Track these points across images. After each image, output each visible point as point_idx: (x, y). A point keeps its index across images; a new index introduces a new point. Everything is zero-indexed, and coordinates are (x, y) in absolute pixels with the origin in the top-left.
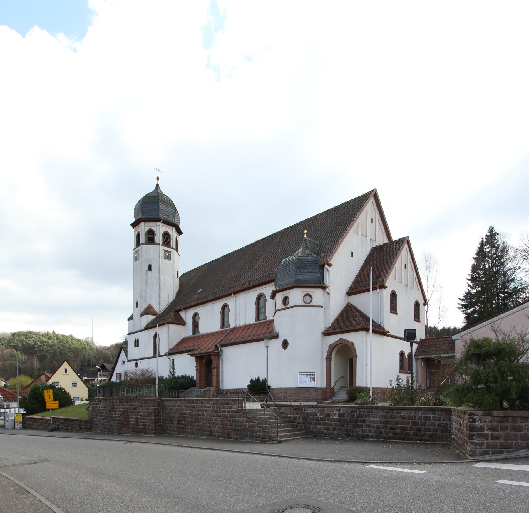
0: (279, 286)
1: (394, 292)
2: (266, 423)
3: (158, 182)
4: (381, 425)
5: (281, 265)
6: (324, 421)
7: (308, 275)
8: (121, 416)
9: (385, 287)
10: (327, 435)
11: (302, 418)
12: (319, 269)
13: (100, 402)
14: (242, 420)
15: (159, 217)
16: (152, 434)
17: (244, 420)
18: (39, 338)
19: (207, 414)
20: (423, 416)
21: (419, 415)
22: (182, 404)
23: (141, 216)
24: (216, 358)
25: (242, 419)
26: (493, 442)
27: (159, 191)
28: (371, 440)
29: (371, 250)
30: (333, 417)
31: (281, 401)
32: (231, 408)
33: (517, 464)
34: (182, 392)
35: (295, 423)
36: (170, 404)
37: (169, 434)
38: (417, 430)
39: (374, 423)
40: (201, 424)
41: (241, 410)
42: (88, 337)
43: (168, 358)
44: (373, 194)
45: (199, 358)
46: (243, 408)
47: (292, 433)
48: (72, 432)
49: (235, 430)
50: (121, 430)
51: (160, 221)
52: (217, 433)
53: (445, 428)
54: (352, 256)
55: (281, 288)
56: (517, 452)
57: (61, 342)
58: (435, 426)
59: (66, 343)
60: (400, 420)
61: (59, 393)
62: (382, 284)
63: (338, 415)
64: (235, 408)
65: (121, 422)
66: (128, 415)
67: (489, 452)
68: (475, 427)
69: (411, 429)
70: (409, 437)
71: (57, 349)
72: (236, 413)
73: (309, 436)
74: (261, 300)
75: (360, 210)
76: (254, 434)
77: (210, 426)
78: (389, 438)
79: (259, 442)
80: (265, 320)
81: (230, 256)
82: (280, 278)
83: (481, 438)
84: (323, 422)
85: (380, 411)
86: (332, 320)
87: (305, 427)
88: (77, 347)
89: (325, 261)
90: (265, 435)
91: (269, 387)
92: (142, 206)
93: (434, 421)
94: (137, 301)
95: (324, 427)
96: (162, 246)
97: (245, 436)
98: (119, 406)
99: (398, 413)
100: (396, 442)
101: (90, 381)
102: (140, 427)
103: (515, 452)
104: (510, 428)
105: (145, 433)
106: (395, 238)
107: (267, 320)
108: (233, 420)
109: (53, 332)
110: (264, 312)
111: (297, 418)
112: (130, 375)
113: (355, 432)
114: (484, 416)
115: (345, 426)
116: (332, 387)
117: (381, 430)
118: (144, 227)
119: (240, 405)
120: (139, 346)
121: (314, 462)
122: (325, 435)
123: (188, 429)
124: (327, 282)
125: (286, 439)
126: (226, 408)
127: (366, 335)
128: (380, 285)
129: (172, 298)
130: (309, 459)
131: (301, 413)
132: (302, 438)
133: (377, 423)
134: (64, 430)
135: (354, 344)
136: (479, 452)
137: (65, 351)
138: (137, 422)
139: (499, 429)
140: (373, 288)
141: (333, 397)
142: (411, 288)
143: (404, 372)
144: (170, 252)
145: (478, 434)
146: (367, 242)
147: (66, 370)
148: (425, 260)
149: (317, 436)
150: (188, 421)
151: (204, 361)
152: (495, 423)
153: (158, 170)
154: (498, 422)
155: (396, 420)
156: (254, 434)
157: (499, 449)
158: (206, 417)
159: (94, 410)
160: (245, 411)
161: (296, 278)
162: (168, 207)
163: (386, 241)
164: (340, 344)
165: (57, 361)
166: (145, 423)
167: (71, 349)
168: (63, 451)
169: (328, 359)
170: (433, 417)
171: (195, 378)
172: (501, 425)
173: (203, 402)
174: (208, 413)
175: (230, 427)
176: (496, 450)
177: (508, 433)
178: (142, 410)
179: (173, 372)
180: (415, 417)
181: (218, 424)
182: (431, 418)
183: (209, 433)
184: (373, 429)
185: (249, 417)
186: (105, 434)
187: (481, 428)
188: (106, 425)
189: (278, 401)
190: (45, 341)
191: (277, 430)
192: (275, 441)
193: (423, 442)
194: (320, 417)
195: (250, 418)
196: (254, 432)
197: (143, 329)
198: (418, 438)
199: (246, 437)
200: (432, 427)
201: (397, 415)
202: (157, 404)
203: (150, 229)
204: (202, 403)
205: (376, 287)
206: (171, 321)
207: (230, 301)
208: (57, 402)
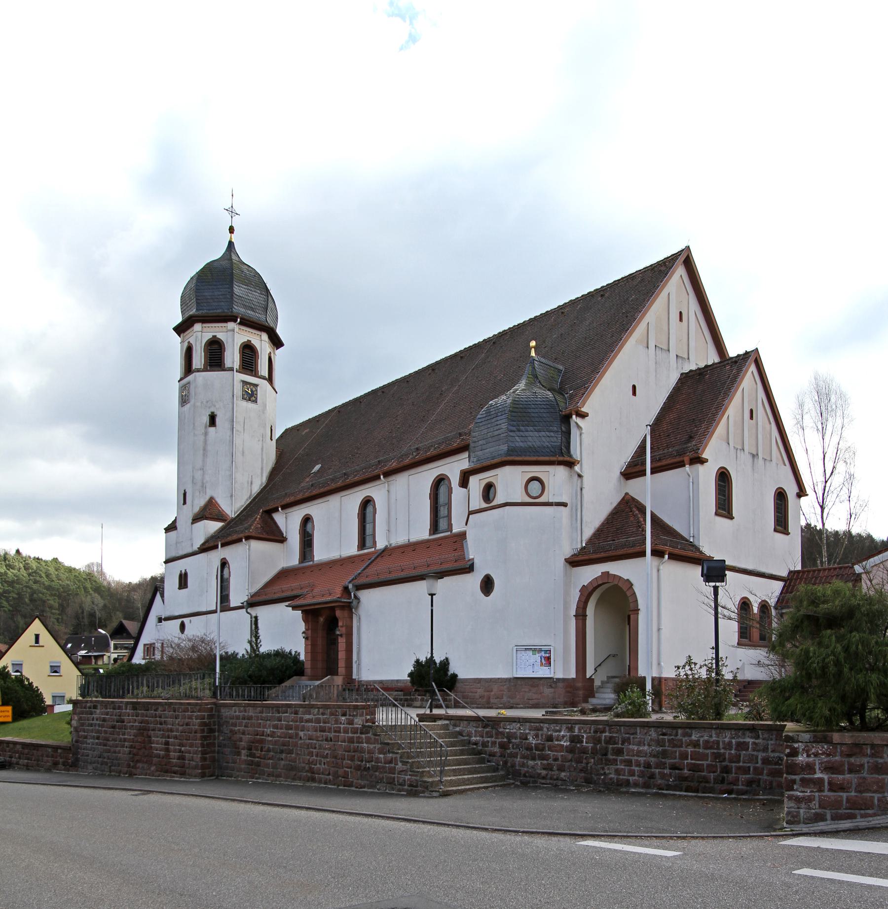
0: (475, 461)
1: (724, 471)
2: (419, 754)
3: (231, 238)
4: (653, 759)
5: (479, 416)
7: (536, 438)
8: (136, 739)
10: (548, 781)
11: (499, 745)
12: (559, 423)
13: (94, 708)
14: (372, 747)
15: (232, 312)
16: (195, 776)
17: (375, 747)
19: (305, 735)
20: (734, 741)
21: (727, 740)
22: (256, 714)
23: (195, 310)
24: (346, 613)
25: (372, 746)
26: (834, 796)
27: (234, 257)
28: (634, 790)
29: (679, 379)
30: (559, 743)
31: (479, 706)
32: (351, 722)
33: (866, 840)
34: (269, 689)
36: (233, 713)
37: (231, 777)
38: (722, 772)
39: (638, 756)
40: (293, 755)
41: (371, 727)
42: (93, 564)
43: (248, 613)
44: (682, 258)
45: (310, 614)
46: (375, 723)
47: (475, 776)
48: (38, 771)
49: (359, 770)
50: (135, 767)
51: (235, 321)
52: (324, 775)
53: (777, 767)
54: (634, 393)
55: (478, 466)
56: (883, 817)
57: (34, 574)
58: (757, 763)
59: (43, 575)
60: (689, 750)
61: (17, 688)
62: (696, 455)
64: (359, 722)
65: (135, 751)
66: (150, 737)
67: (826, 815)
68: (796, 765)
69: (711, 769)
70: (707, 785)
71: (25, 589)
72: (361, 733)
73: (511, 781)
74: (443, 489)
75: (651, 296)
76: (394, 778)
77: (311, 760)
78: (669, 788)
79: (405, 793)
80: (449, 533)
81: (383, 392)
82: (477, 444)
83: (810, 788)
85: (651, 731)
86: (588, 532)
87: (505, 763)
88: (68, 585)
89: (571, 407)
90: (416, 780)
91: (455, 676)
92: (196, 289)
93: (755, 753)
94: (185, 491)
95: (541, 763)
96: (240, 372)
97: (378, 782)
98: (132, 716)
99: (684, 735)
100: (680, 796)
101: (93, 661)
102: (173, 762)
103: (879, 816)
104: (869, 767)
105: (183, 774)
106: (733, 351)
107: (454, 531)
108: (354, 747)
109: (18, 551)
110: (447, 514)
111: (490, 744)
112: (169, 651)
113: (602, 775)
114: (814, 742)
115: (582, 762)
116: (588, 677)
117: (652, 770)
118: (201, 334)
119: (368, 717)
120: (187, 587)
121: (484, 834)
122: (543, 781)
123: (267, 766)
124: (576, 450)
125: (460, 788)
126: (341, 723)
127: (659, 566)
128: (692, 457)
129: (260, 483)
130: (478, 828)
131: (499, 734)
132: (495, 786)
133: (645, 757)
134: (22, 767)
135: (632, 585)
136: (805, 817)
137: (41, 593)
138: (167, 750)
139: (846, 769)
140: (651, 469)
142: (765, 459)
143: (750, 643)
144: (256, 385)
145: (802, 780)
146: (669, 362)
147: (37, 637)
148: (816, 394)
149: (529, 782)
150: (269, 750)
151: (322, 619)
152: (837, 758)
153: (232, 211)
154: (842, 754)
155: (682, 749)
156: (394, 778)
157: (845, 809)
158: (303, 741)
159: (82, 725)
160: (379, 730)
161: (510, 444)
162: (253, 289)
163: (713, 358)
164: (604, 584)
165: (24, 616)
166: (183, 752)
167: (53, 589)
168: (7, 811)
169: (580, 616)
170: (754, 743)
171: (302, 657)
172: (848, 762)
173: (298, 709)
174: (306, 732)
175: (349, 762)
176: (840, 811)
177: (864, 778)
178: (177, 727)
179: (257, 644)
180: (718, 743)
181: (326, 757)
182: (750, 747)
183: (309, 774)
184: (637, 769)
185: (386, 741)
186: (102, 776)
187: (810, 768)
188: (104, 758)
191: (439, 769)
192: (436, 791)
193: (733, 796)
194: (534, 742)
195: (388, 744)
196: (394, 774)
197: (197, 550)
198: (725, 787)
199: (380, 784)
200: (752, 766)
201: (684, 739)
202: (206, 714)
203: (214, 337)
204: (296, 713)
205: (683, 461)
206: (253, 534)
207: (377, 492)
208: (9, 708)
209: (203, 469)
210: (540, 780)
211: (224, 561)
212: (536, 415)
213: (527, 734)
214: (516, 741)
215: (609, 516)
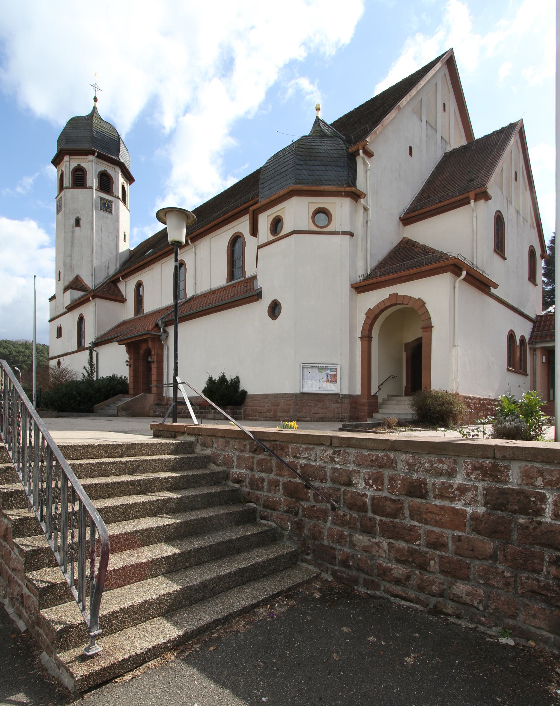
3: (95, 105)
6: (395, 516)
9: (486, 197)
10: (412, 594)
11: (284, 488)
18: (15, 347)
30: (446, 503)
31: (267, 419)
35: (257, 502)
44: (446, 58)
51: (94, 154)
54: (411, 154)
62: (482, 190)
63: (480, 498)
82: (266, 184)
84: (384, 519)
87: (299, 526)
91: (244, 393)
95: (390, 544)
111: (265, 484)
115: (539, 572)
116: (372, 394)
122: (397, 589)
141: (374, 415)
146: (437, 140)
153: (96, 87)
189: (261, 420)
190: (21, 351)
209: (71, 256)
210: (388, 585)
211: (81, 316)
212: (323, 151)
213: (350, 474)
214: (323, 485)
215: (390, 253)
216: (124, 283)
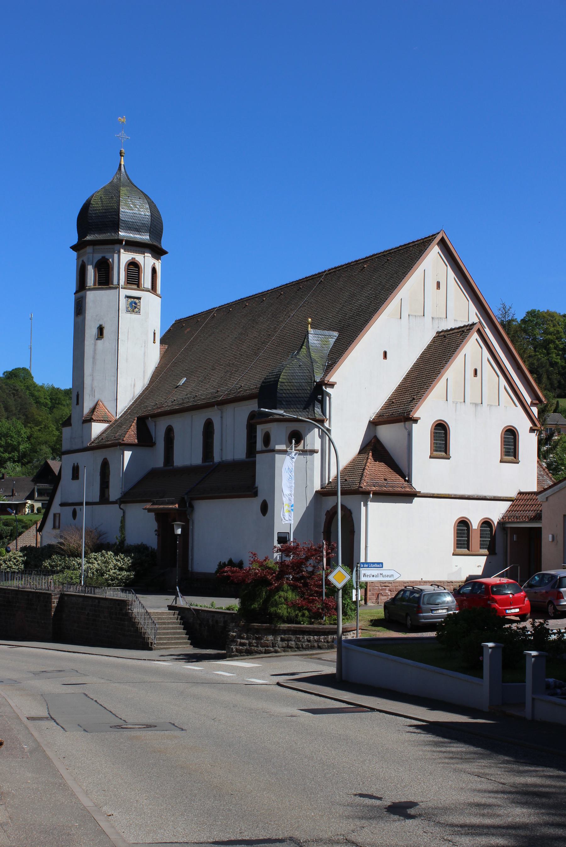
43: (121, 509)
142: (491, 406)
144: (139, 298)
216: (154, 424)
